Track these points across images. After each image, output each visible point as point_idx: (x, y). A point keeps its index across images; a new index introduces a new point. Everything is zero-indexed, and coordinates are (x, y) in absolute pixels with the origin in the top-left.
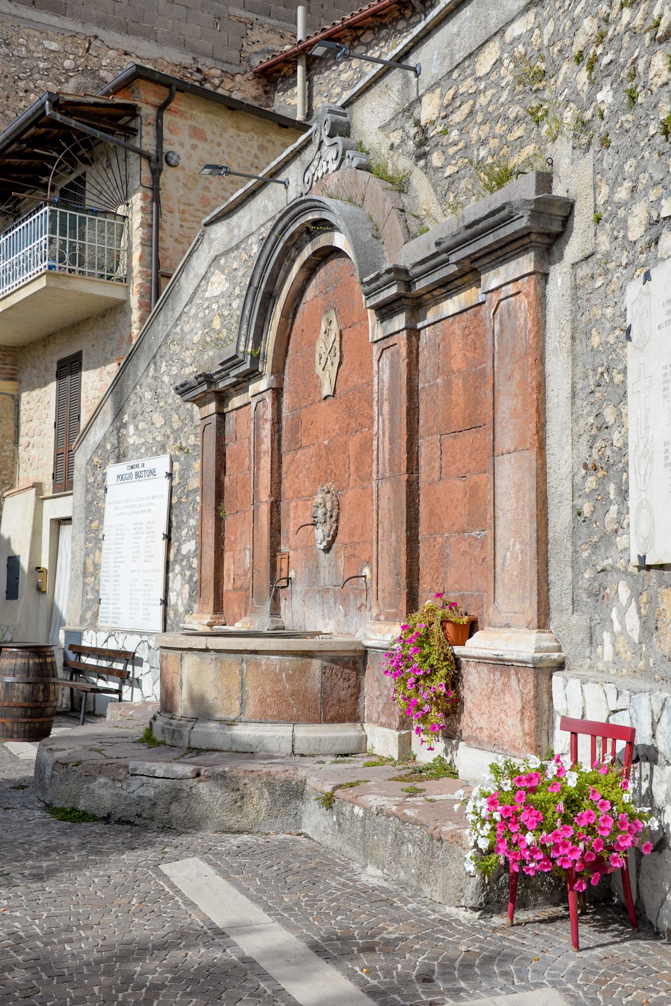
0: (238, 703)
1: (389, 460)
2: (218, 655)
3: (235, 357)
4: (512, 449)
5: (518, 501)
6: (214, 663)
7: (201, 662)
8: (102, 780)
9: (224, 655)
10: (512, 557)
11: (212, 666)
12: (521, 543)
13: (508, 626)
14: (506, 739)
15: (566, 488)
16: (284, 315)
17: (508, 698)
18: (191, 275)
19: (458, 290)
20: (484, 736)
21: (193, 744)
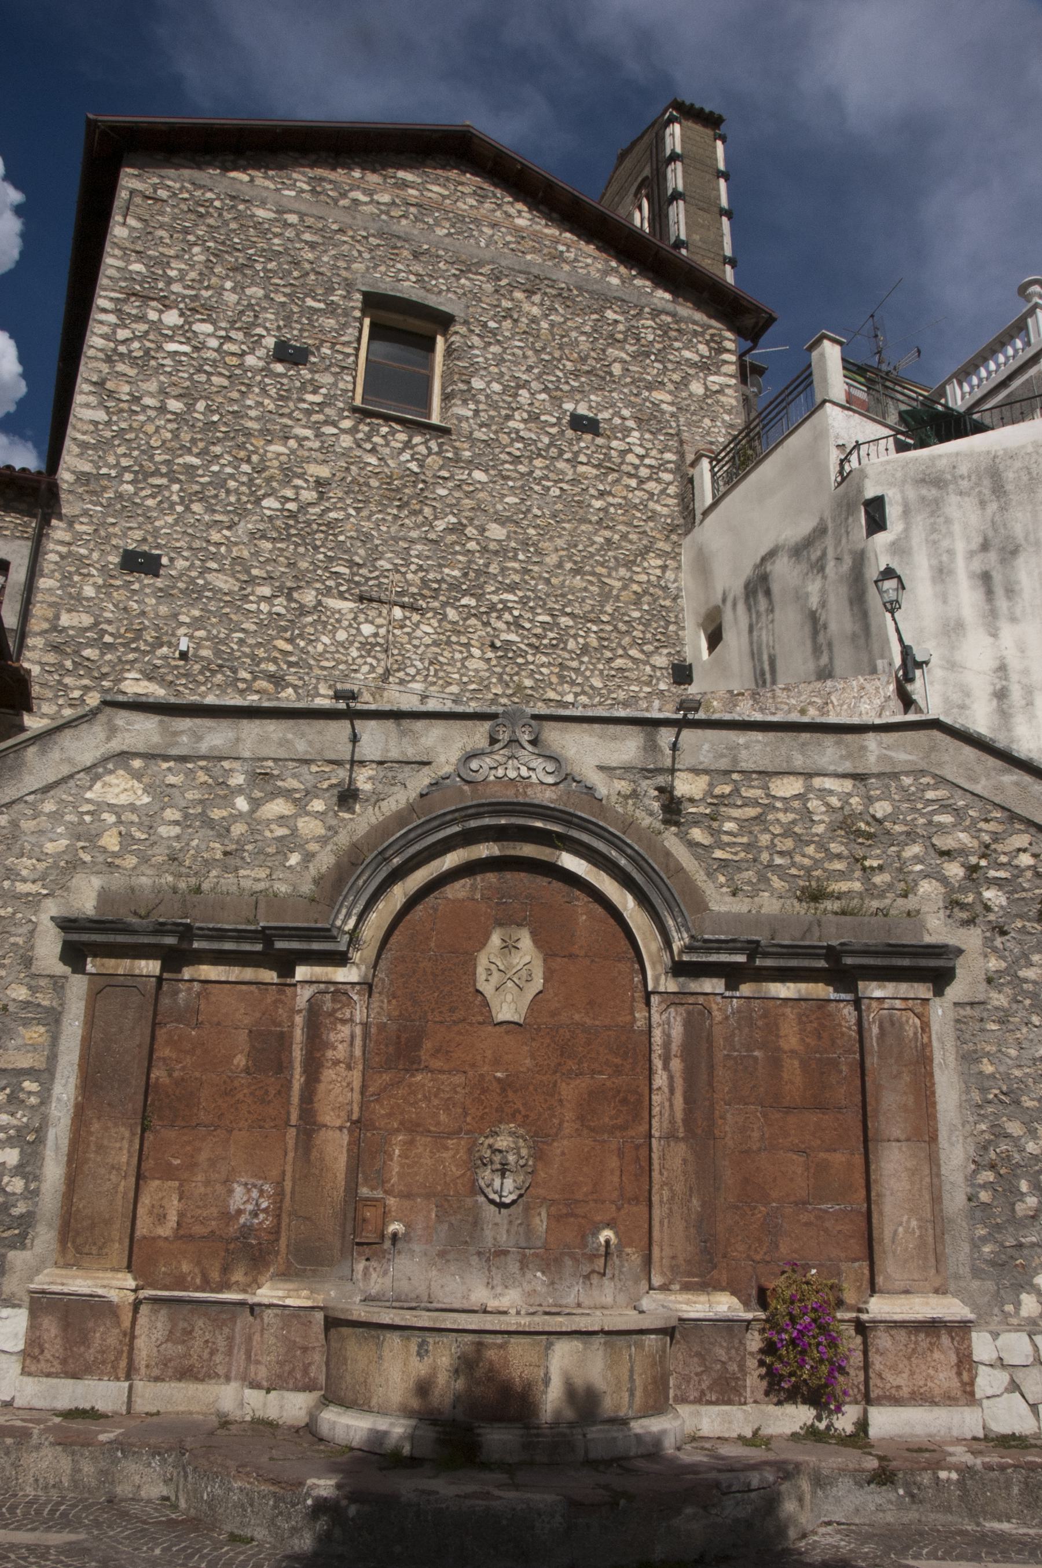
0: (627, 1394)
1: (684, 1121)
2: (608, 1338)
3: (329, 930)
4: (903, 1137)
5: (912, 1183)
6: (602, 1348)
7: (585, 1349)
8: (689, 1510)
9: (615, 1337)
10: (906, 1232)
11: (601, 1353)
12: (919, 1220)
13: (907, 1292)
14: (937, 1391)
15: (958, 1178)
16: (718, 951)
17: (937, 1355)
18: (56, 755)
19: (816, 980)
20: (905, 1392)
21: (592, 1455)
